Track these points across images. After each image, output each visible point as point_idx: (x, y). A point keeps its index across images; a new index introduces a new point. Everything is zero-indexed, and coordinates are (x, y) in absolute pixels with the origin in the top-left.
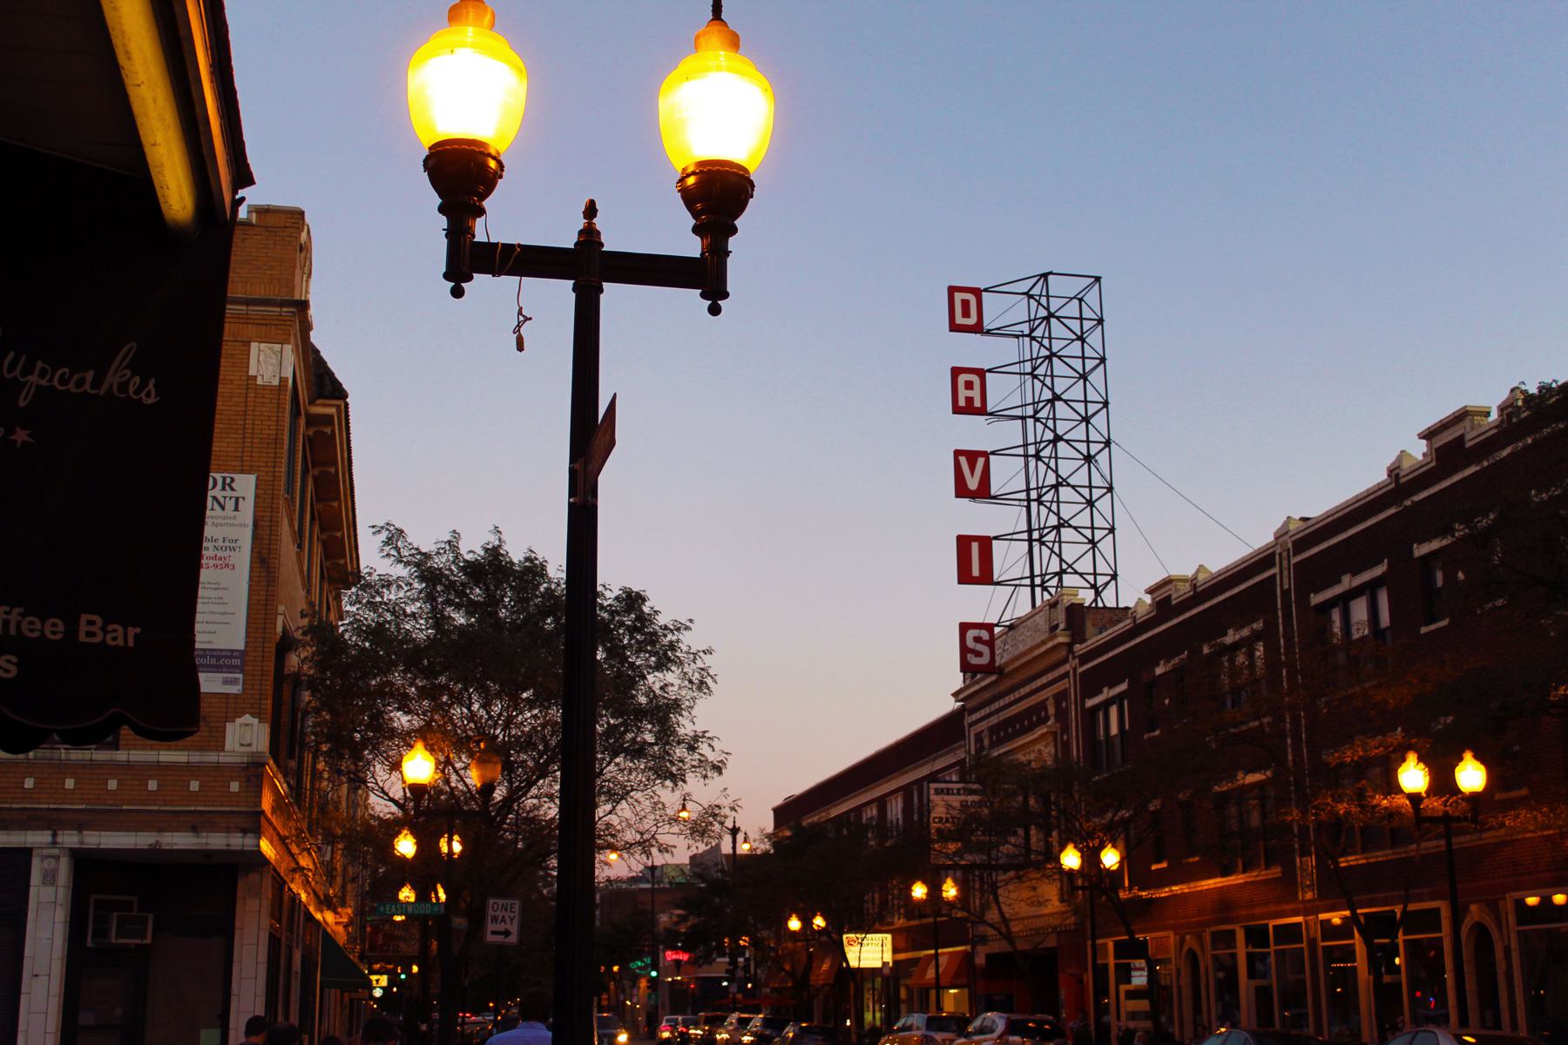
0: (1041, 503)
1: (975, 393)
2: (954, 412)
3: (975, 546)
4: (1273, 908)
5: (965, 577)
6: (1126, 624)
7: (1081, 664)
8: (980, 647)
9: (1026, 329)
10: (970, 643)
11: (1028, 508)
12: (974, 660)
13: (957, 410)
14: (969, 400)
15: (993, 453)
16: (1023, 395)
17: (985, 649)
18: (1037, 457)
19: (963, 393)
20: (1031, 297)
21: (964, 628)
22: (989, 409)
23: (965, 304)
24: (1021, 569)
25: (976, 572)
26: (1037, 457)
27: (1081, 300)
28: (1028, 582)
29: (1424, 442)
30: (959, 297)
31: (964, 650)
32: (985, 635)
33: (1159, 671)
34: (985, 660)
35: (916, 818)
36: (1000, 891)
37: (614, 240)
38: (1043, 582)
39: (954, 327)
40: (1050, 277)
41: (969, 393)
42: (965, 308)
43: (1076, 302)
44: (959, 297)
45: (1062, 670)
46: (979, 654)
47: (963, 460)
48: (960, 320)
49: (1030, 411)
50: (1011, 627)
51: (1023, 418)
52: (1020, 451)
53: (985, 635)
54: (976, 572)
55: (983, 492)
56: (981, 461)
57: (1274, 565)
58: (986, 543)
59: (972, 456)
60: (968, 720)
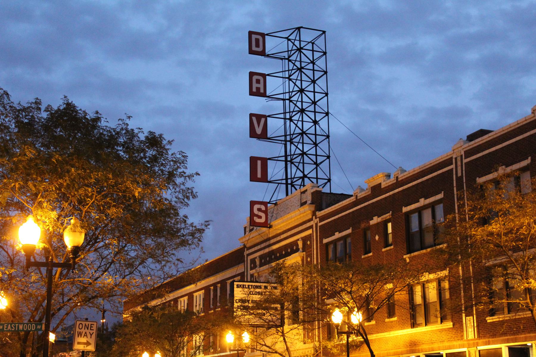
0: (292, 143)
1: (261, 86)
3: (259, 162)
4: (446, 344)
5: (253, 178)
6: (352, 199)
7: (321, 221)
8: (261, 214)
9: (286, 55)
10: (256, 212)
12: (257, 220)
13: (252, 93)
14: (258, 89)
15: (269, 116)
16: (284, 88)
17: (263, 215)
18: (291, 120)
19: (255, 85)
20: (289, 40)
22: (268, 94)
23: (257, 41)
24: (281, 175)
25: (259, 175)
26: (291, 120)
27: (313, 44)
28: (284, 182)
30: (254, 37)
31: (252, 215)
32: (263, 208)
33: (372, 222)
34: (263, 220)
38: (292, 182)
39: (251, 52)
40: (301, 29)
41: (258, 85)
43: (311, 44)
45: (308, 225)
47: (254, 119)
48: (254, 48)
49: (287, 96)
50: (276, 204)
51: (284, 100)
52: (282, 116)
53: (263, 208)
54: (259, 175)
55: (263, 136)
56: (263, 120)
57: (452, 164)
58: (264, 161)
59: (259, 117)
60: (246, 252)
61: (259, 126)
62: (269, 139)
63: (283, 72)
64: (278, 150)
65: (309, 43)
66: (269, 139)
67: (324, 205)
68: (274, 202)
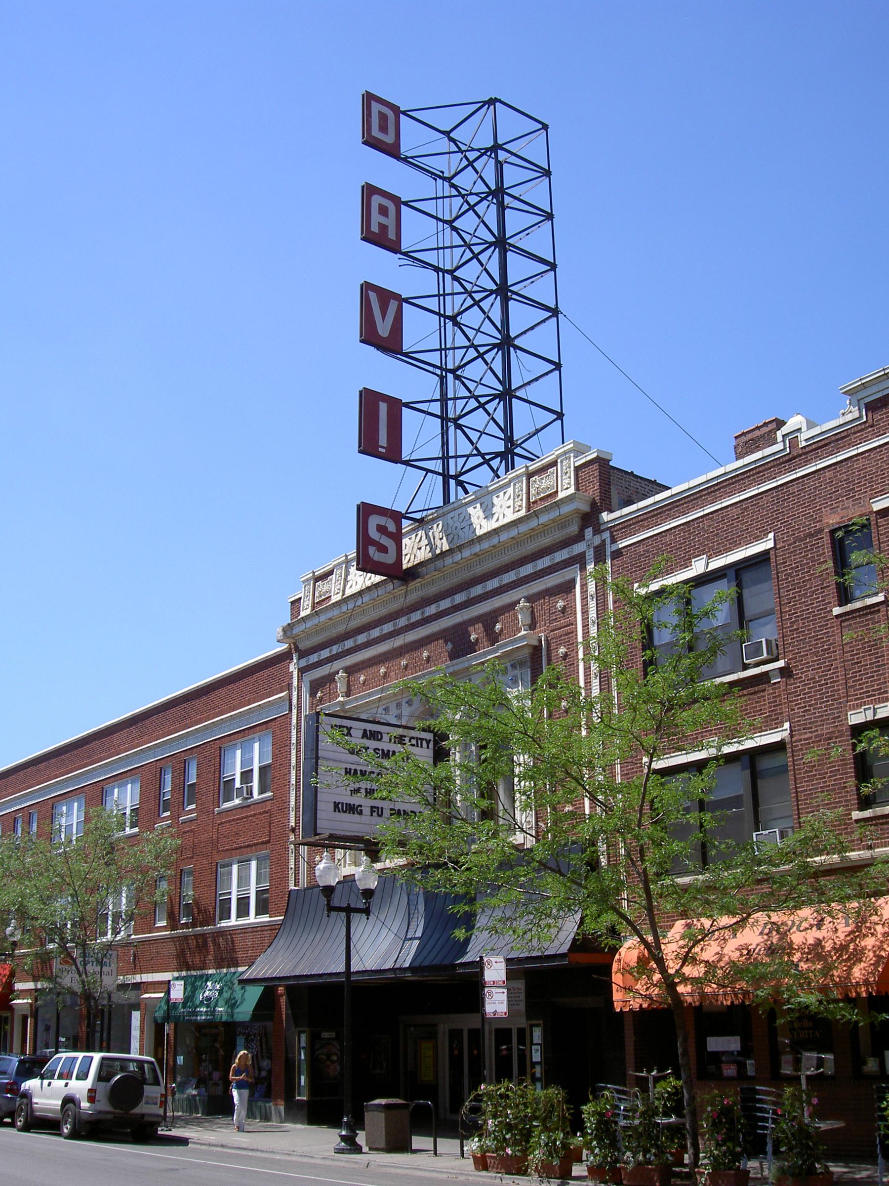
1: (390, 222)
3: (383, 407)
8: (385, 541)
10: (373, 533)
14: (383, 228)
19: (376, 218)
21: (365, 511)
34: (389, 558)
36: (405, 541)
37: (353, 906)
41: (383, 220)
42: (381, 126)
44: (376, 200)
46: (383, 549)
47: (373, 296)
53: (391, 527)
56: (393, 305)
58: (396, 406)
59: (386, 296)
62: (406, 355)
63: (438, 249)
67: (615, 500)
68: (418, 516)
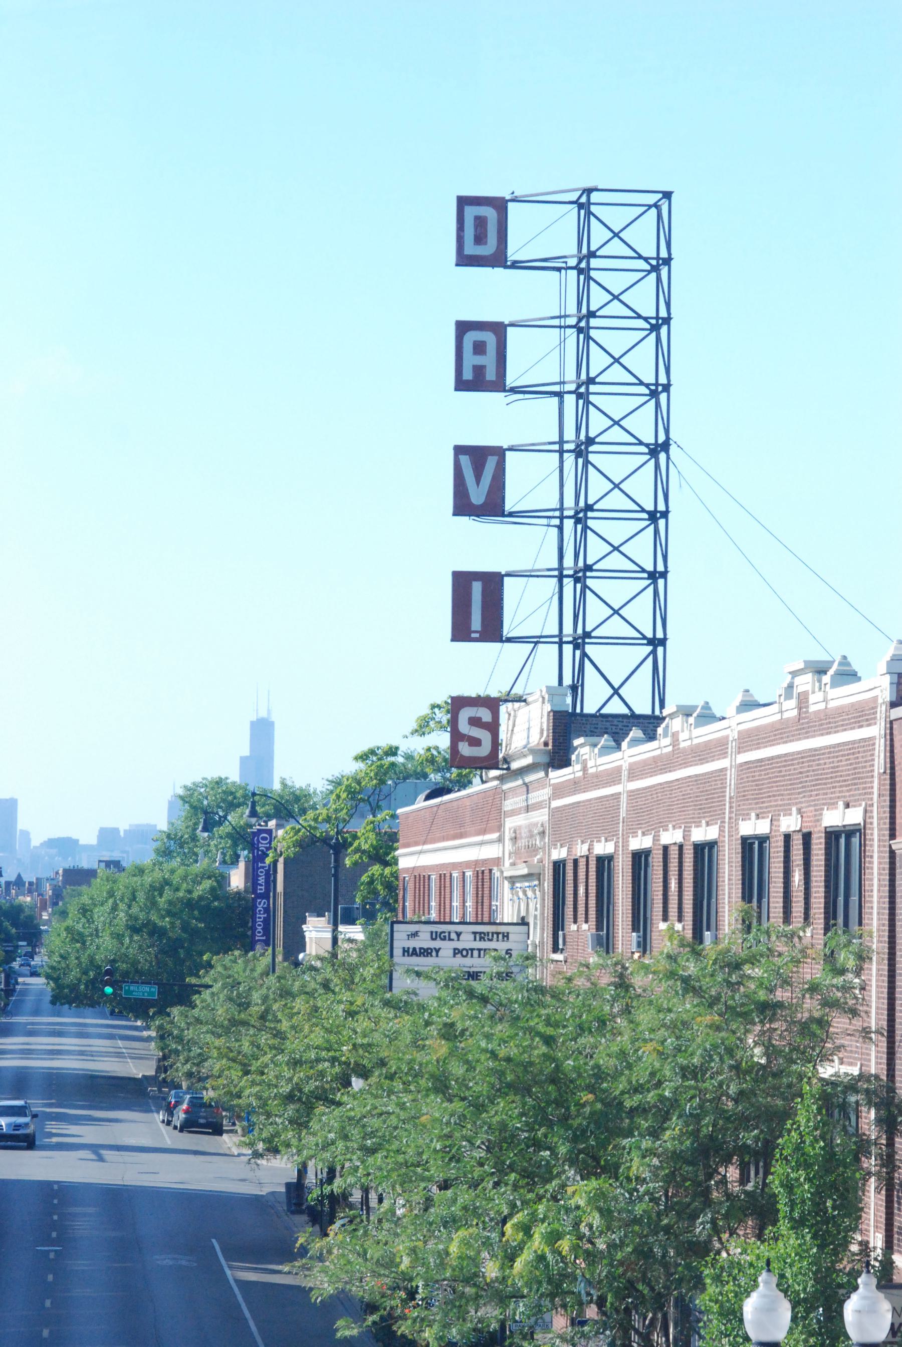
1: (489, 360)
2: (457, 389)
8: (476, 732)
11: (560, 528)
14: (479, 370)
29: (790, 676)
34: (485, 750)
35: (761, 1164)
41: (479, 360)
42: (482, 232)
44: (471, 212)
46: (475, 742)
53: (485, 715)
55: (493, 507)
56: (491, 463)
58: (493, 583)
61: (478, 483)
62: (511, 515)
64: (548, 294)
65: (650, 207)
66: (511, 515)
